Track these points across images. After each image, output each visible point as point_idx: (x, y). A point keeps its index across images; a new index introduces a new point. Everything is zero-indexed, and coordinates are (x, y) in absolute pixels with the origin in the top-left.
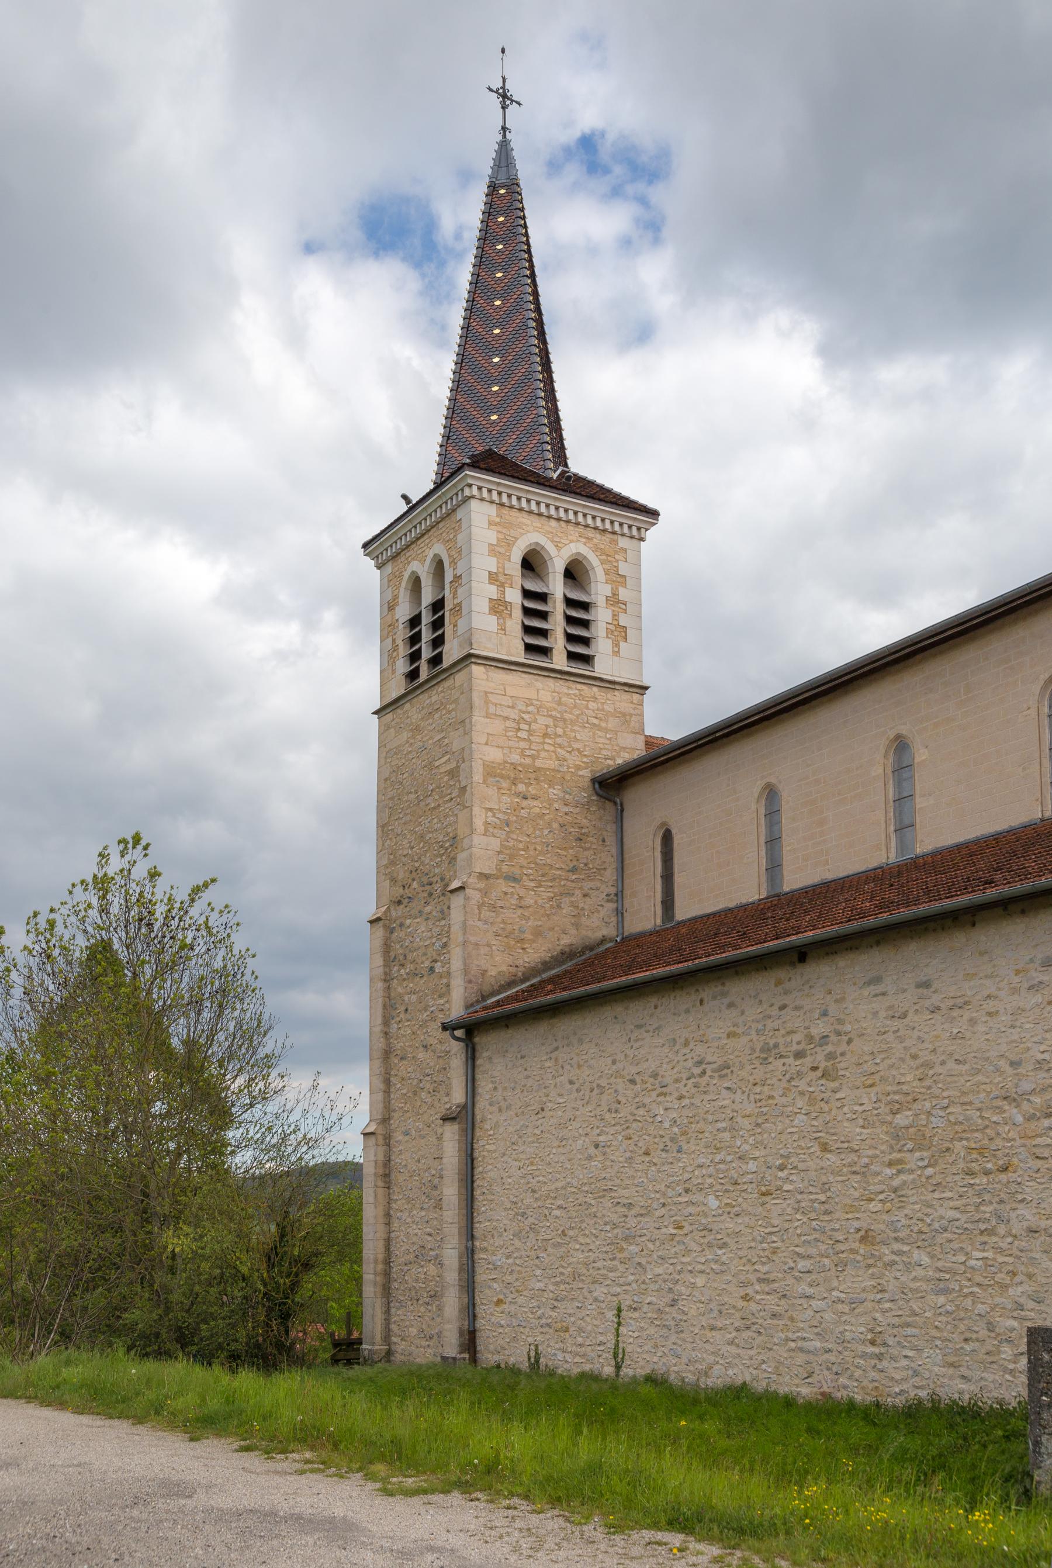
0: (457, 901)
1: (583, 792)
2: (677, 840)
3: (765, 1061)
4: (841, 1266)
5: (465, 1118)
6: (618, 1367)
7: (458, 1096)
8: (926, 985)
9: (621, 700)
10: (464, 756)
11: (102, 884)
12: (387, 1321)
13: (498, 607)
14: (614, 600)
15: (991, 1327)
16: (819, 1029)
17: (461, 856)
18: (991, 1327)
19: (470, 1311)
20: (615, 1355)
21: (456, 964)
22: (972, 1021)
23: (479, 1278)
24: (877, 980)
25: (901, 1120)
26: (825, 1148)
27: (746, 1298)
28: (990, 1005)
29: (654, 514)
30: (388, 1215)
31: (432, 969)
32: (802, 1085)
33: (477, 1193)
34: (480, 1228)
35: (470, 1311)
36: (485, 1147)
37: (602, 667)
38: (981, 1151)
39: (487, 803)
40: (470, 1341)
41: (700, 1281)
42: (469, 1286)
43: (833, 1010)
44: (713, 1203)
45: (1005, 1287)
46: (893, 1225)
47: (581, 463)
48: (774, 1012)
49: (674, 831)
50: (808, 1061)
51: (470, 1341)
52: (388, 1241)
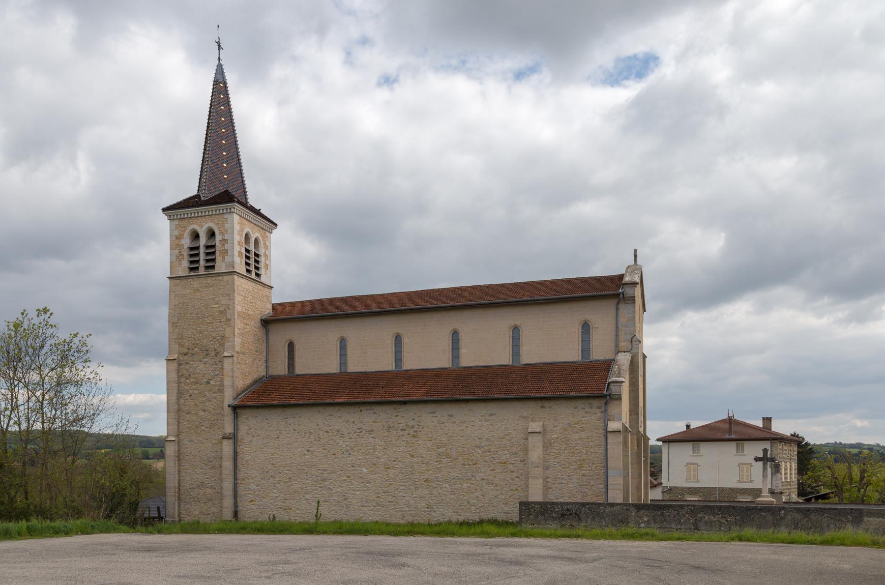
0: (226, 361)
1: (259, 324)
2: (297, 347)
3: (388, 431)
4: (417, 488)
5: (234, 438)
6: (317, 519)
7: (229, 429)
8: (452, 416)
9: (266, 290)
10: (230, 307)
11: (17, 326)
12: (179, 509)
13: (240, 253)
14: (265, 255)
15: (468, 502)
16: (411, 423)
17: (227, 344)
18: (468, 502)
19: (236, 505)
20: (316, 516)
21: (227, 382)
22: (467, 427)
23: (239, 493)
24: (434, 412)
25: (440, 450)
26: (412, 456)
27: (378, 497)
28: (473, 423)
29: (276, 225)
30: (179, 471)
31: (208, 383)
32: (404, 438)
33: (239, 464)
34: (239, 476)
35: (236, 505)
36: (243, 449)
37: (263, 279)
38: (468, 460)
39: (239, 324)
40: (236, 514)
41: (358, 493)
42: (235, 496)
43: (416, 419)
44: (365, 470)
45: (473, 493)
46: (437, 478)
47: (252, 201)
48: (393, 417)
49: (295, 343)
50: (407, 432)
51: (236, 514)
52: (179, 480)
